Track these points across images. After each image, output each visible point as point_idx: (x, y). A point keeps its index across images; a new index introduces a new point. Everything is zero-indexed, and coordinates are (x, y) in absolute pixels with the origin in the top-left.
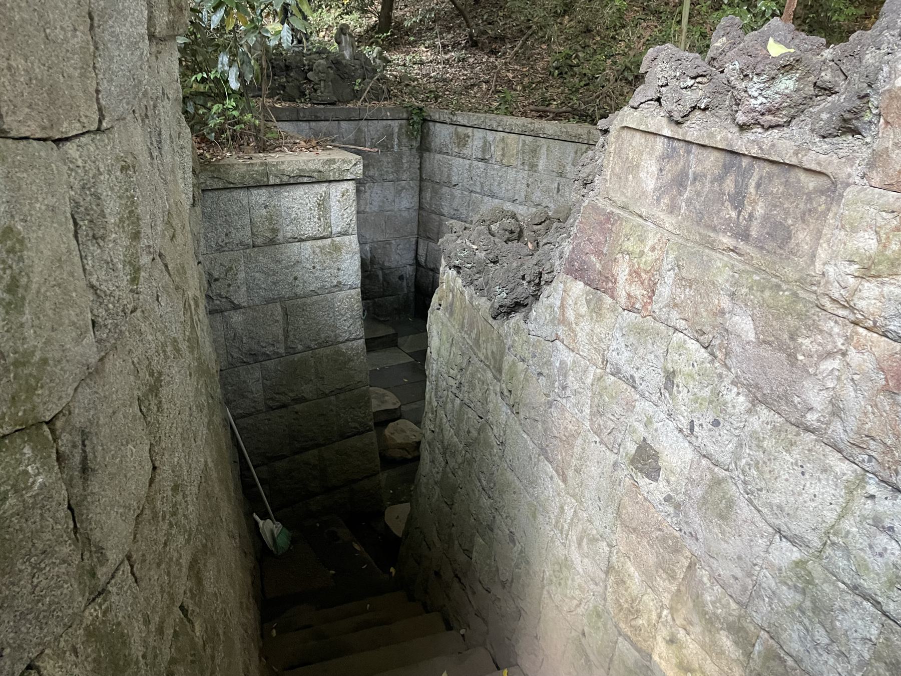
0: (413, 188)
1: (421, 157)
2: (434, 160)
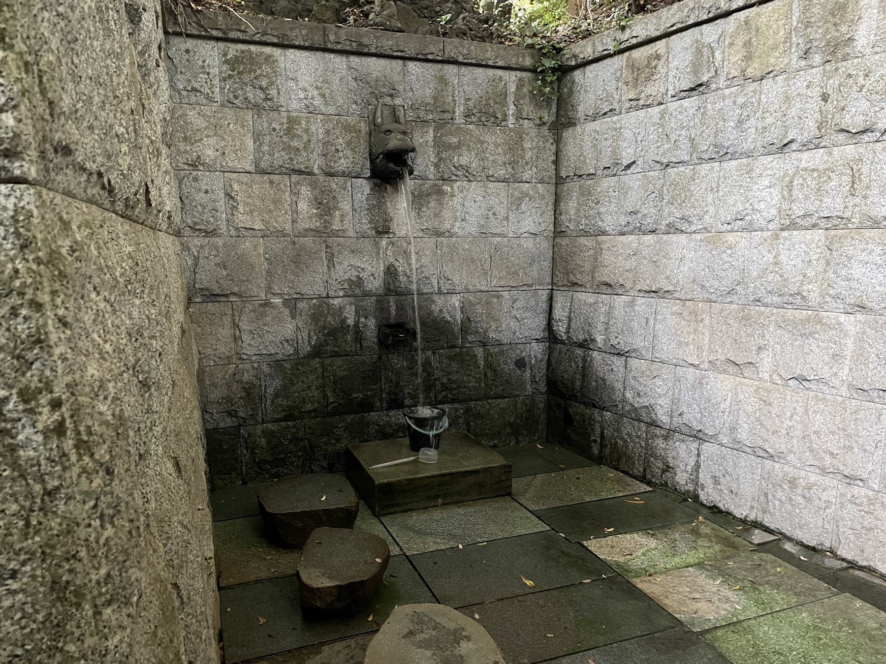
0: (543, 197)
1: (558, 141)
2: (585, 142)
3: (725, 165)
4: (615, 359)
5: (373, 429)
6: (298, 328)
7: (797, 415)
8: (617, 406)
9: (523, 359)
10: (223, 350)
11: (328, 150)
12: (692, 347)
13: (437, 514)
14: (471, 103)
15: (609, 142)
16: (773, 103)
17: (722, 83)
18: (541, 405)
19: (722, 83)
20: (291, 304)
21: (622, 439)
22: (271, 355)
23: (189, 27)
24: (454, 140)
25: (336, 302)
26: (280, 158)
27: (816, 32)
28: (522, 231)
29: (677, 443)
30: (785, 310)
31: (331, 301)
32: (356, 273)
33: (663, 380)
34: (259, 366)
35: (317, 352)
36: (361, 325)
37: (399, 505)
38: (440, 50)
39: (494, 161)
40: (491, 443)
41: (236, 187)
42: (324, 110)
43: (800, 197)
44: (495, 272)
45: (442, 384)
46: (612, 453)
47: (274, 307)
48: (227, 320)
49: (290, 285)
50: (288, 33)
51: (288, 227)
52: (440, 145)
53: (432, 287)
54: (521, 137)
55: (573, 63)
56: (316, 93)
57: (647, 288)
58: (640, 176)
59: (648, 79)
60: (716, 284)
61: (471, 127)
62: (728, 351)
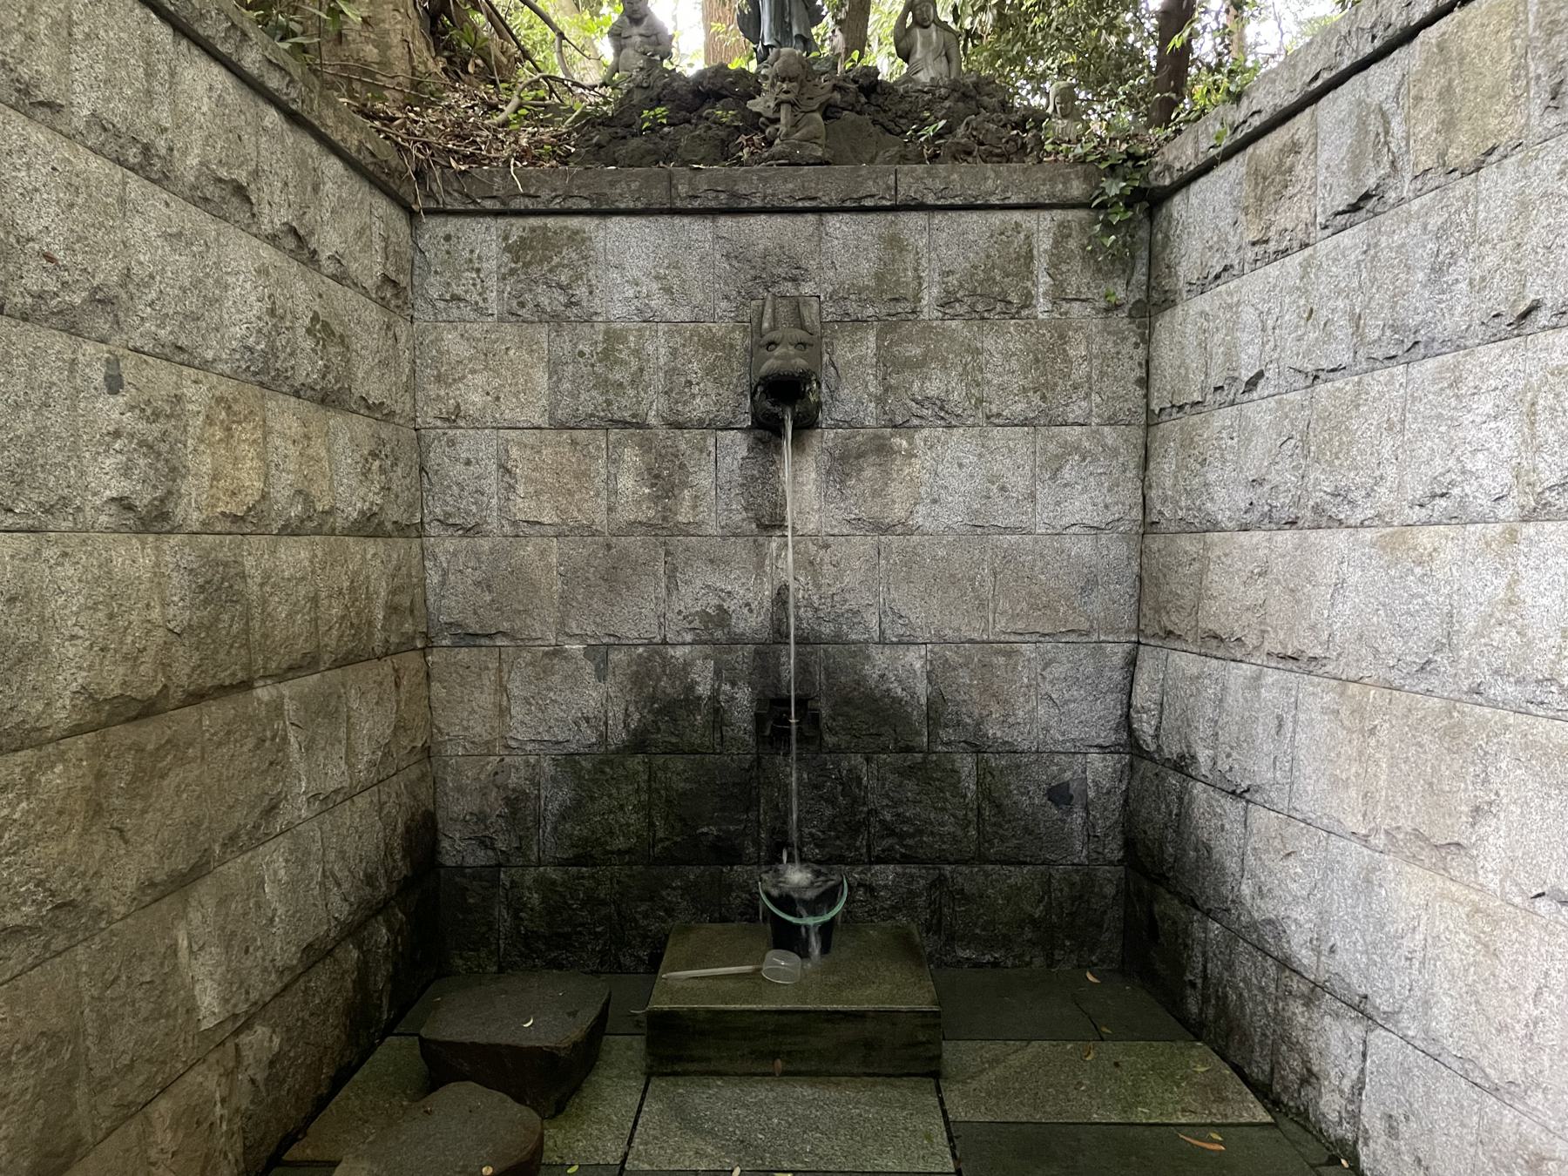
1: (1146, 340)
2: (1192, 337)
3: (1415, 369)
4: (1228, 803)
5: (737, 899)
6: (609, 698)
7: (1552, 992)
8: (1228, 910)
9: (1067, 785)
10: (480, 730)
11: (677, 384)
13: (761, 1092)
14: (953, 280)
15: (1220, 335)
16: (1496, 220)
17: (1407, 188)
18: (1110, 890)
19: (1407, 188)
20: (599, 654)
21: (1235, 988)
22: (558, 743)
23: (448, 200)
24: (915, 351)
25: (679, 652)
26: (591, 400)
29: (1327, 1019)
30: (1531, 720)
31: (671, 651)
32: (716, 602)
33: (1304, 864)
34: (538, 761)
35: (639, 743)
36: (722, 698)
37: (692, 1060)
38: (889, 188)
40: (988, 957)
41: (514, 452)
42: (670, 315)
43: (1551, 438)
44: (1003, 604)
46: (1217, 1018)
48: (489, 679)
51: (600, 518)
52: (888, 362)
53: (867, 630)
54: (1061, 337)
55: (1167, 182)
56: (655, 286)
57: (1279, 649)
58: (1272, 403)
59: (1279, 195)
60: (1398, 645)
61: (954, 324)
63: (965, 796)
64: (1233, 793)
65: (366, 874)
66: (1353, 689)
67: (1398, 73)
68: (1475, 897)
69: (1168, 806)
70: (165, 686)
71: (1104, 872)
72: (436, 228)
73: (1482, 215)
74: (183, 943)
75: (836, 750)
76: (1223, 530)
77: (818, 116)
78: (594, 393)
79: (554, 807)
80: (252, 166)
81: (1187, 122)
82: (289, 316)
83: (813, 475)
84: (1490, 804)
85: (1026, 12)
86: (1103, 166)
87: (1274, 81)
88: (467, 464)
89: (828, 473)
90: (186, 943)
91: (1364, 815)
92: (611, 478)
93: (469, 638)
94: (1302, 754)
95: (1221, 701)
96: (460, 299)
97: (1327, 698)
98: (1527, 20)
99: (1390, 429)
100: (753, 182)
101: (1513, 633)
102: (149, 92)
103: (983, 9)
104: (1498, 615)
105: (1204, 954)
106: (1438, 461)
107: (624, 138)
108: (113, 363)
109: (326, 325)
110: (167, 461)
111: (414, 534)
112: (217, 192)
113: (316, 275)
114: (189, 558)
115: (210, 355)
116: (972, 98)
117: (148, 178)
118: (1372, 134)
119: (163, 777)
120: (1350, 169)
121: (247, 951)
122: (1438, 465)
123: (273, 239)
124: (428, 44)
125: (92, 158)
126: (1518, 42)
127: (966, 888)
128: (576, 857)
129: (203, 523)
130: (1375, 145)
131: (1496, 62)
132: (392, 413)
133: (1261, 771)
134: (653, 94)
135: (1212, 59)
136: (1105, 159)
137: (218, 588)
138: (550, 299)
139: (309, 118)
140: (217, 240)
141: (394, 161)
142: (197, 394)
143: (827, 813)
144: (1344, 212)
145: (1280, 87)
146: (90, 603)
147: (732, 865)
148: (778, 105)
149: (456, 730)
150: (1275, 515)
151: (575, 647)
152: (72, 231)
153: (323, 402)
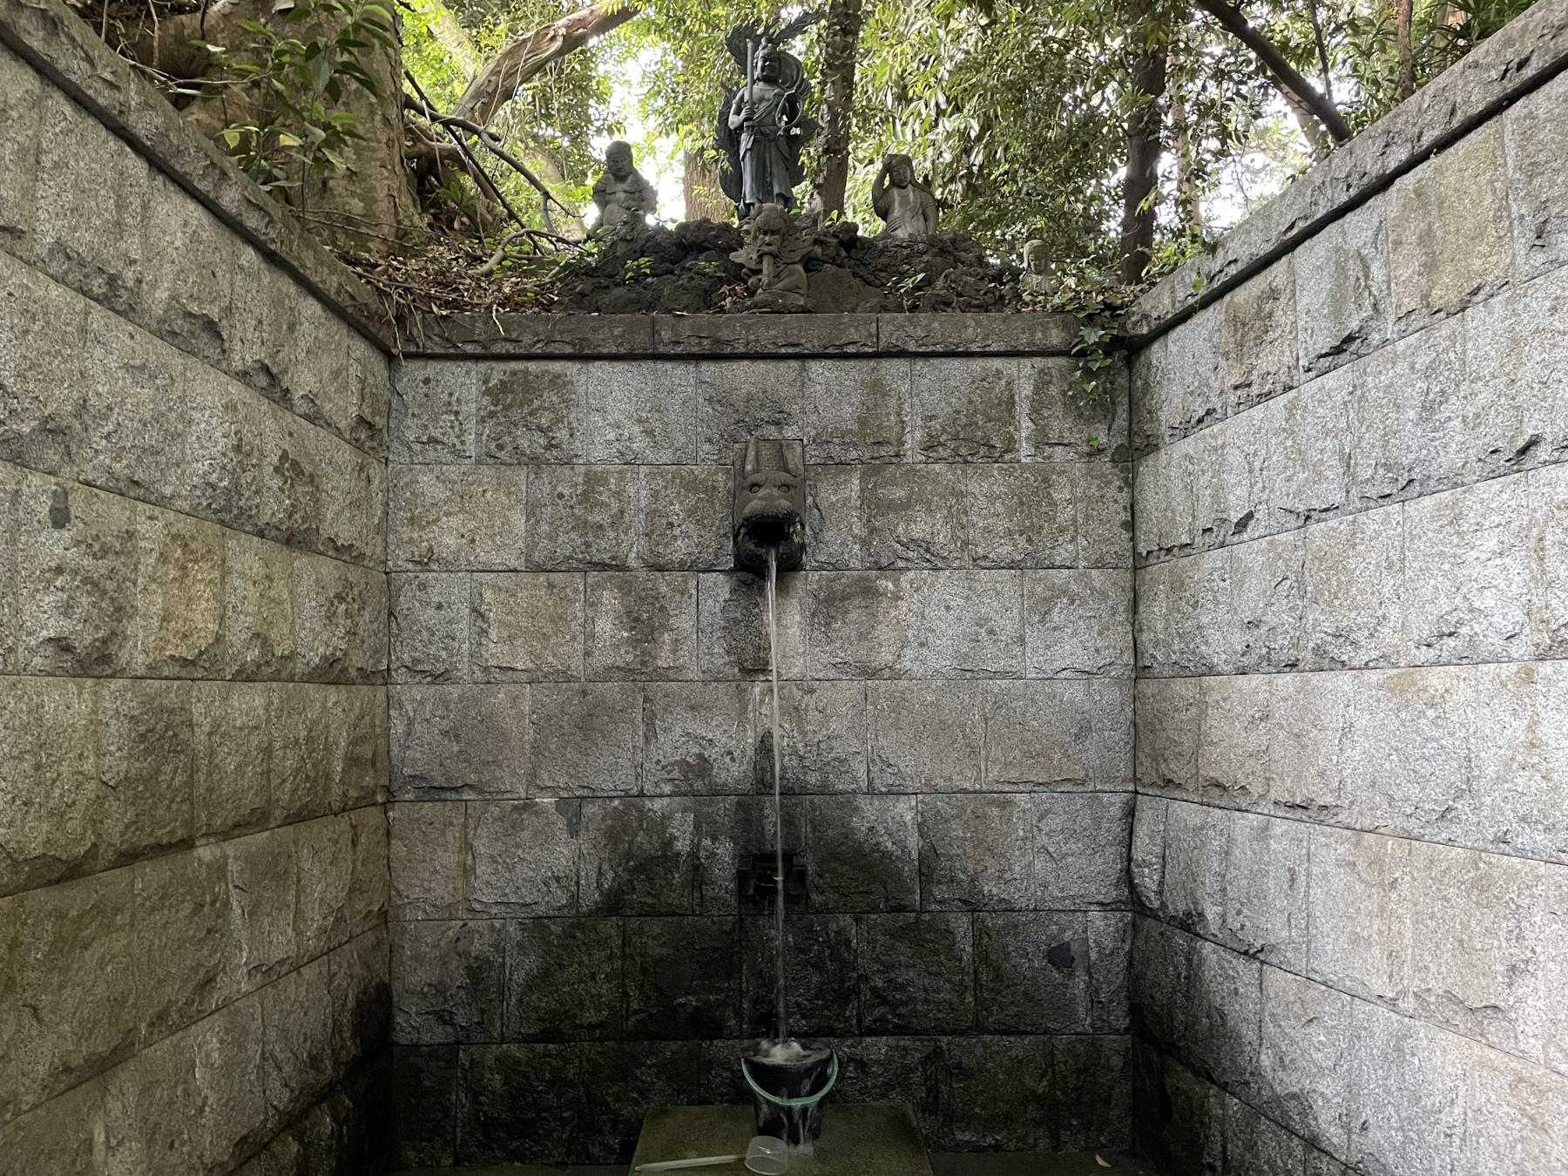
0: (1104, 596)
1: (1131, 484)
2: (1178, 481)
3: (1411, 507)
4: (1240, 964)
8: (1247, 1083)
10: (442, 891)
12: (1376, 951)
15: (1207, 477)
17: (1391, 330)
18: (1117, 1061)
19: (1391, 330)
20: (571, 808)
22: (526, 905)
23: (429, 344)
24: (899, 493)
25: (657, 805)
26: (569, 543)
27: (1553, 184)
28: (1057, 665)
31: (648, 804)
33: (1329, 1031)
34: (504, 926)
35: (613, 904)
36: (702, 854)
39: (987, 530)
40: (989, 1140)
41: (489, 596)
42: (651, 457)
44: (995, 752)
45: (874, 989)
47: (538, 812)
48: (453, 835)
49: (571, 771)
50: (589, 336)
51: (576, 663)
52: (873, 505)
53: (855, 779)
54: (1045, 480)
55: (1145, 330)
56: (637, 429)
57: (1287, 797)
58: (1264, 543)
59: (1259, 341)
60: (1414, 791)
61: (937, 467)
62: (1449, 971)
63: (961, 960)
64: (1246, 953)
65: (310, 1056)
66: (1369, 839)
67: (1375, 221)
68: (1515, 1064)
69: (1176, 968)
70: (94, 845)
71: (1110, 1042)
72: (415, 371)
73: (1471, 354)
74: (100, 1137)
75: (825, 910)
76: (1219, 674)
77: (799, 267)
78: (573, 535)
79: (519, 977)
80: (225, 303)
81: (1161, 274)
82: (256, 453)
83: (798, 618)
84: (1527, 962)
85: (995, 180)
86: (1081, 315)
87: (1248, 232)
88: (439, 611)
89: (813, 615)
90: (102, 1138)
91: (1390, 977)
92: (589, 621)
93: (433, 792)
94: (1318, 911)
95: (1227, 853)
96: (437, 442)
97: (1341, 850)
98: (1506, 164)
99: (1390, 568)
100: (736, 328)
101: (1538, 777)
102: (118, 224)
103: (952, 180)
104: (1520, 758)
105: (1223, 1133)
106: (1443, 599)
107: (607, 287)
108: (61, 496)
109: (295, 464)
110: (112, 599)
111: (380, 681)
112: (187, 327)
113: (288, 414)
114: (132, 705)
115: (168, 491)
116: (950, 253)
117: (113, 309)
118: (1351, 279)
119: (86, 946)
120: (1331, 313)
121: (172, 1146)
122: (1444, 605)
123: (243, 376)
124: (414, 201)
125: (52, 285)
126: (1498, 185)
127: (965, 1061)
128: (541, 1032)
129: (149, 667)
130: (1356, 289)
131: (1476, 204)
132: (362, 556)
133: (1275, 929)
134: (637, 246)
135: (1176, 223)
136: (1082, 308)
137: (160, 737)
138: (528, 441)
139: (288, 258)
140: (183, 374)
141: (374, 305)
142: (151, 529)
143: (815, 980)
144: (1327, 355)
145: (1256, 237)
146: (15, 752)
147: (712, 1039)
148: (761, 257)
149: (416, 893)
150: (1274, 656)
151: (547, 801)
152: (25, 357)
153: (288, 542)
